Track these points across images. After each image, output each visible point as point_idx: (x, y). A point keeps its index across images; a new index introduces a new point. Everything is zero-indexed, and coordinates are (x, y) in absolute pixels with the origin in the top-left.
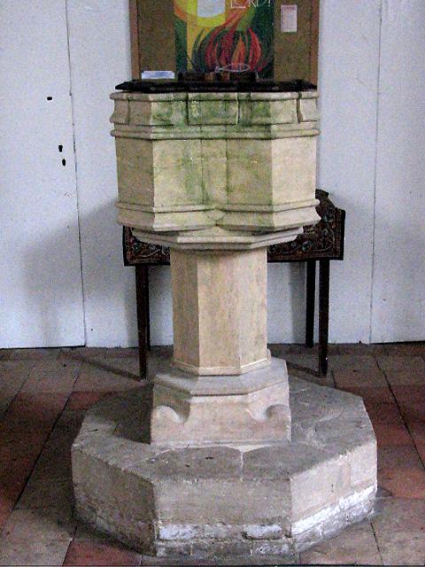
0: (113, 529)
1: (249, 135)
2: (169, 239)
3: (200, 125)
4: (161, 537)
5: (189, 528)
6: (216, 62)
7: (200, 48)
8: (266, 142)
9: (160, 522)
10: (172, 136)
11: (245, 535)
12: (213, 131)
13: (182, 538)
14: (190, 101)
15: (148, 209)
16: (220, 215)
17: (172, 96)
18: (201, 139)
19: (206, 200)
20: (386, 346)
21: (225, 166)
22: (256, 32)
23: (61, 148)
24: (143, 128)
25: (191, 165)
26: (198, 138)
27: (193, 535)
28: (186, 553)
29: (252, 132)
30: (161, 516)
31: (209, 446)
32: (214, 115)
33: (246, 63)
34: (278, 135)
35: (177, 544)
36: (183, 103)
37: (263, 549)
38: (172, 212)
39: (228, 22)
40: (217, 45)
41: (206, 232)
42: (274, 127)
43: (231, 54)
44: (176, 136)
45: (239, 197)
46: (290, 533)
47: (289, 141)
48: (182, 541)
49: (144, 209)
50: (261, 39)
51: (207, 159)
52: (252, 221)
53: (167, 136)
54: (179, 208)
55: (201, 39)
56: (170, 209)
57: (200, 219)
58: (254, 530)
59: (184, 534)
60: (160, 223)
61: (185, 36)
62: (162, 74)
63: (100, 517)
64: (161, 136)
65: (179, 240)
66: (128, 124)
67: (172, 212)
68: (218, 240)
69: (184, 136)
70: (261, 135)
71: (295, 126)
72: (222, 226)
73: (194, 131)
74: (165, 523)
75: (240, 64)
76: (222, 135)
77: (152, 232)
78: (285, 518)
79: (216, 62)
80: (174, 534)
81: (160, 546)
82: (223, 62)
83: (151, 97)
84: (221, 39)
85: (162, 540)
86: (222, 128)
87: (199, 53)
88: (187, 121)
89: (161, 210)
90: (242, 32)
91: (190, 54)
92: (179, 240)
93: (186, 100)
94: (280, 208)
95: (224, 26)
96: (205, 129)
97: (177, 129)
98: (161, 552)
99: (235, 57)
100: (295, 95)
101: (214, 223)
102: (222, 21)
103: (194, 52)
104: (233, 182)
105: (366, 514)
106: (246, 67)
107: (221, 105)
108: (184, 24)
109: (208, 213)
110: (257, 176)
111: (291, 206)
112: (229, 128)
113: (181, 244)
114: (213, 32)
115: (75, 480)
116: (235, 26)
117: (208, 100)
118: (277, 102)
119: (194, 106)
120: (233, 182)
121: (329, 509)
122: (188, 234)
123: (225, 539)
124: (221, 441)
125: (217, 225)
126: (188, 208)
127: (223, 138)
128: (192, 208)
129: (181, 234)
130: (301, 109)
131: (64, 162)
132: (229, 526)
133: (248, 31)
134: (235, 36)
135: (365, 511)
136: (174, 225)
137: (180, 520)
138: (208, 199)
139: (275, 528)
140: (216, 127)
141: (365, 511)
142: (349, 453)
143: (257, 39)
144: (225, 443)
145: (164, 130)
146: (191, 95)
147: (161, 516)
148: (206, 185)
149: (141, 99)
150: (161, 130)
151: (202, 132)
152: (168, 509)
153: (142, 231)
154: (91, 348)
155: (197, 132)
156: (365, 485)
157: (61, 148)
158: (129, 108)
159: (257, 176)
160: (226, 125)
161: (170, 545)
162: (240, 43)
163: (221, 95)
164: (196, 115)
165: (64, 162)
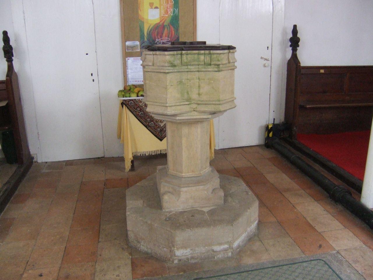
0: (149, 251)
1: (209, 70)
2: (174, 118)
3: (187, 65)
4: (176, 255)
5: (188, 250)
6: (156, 37)
7: (150, 31)
8: (217, 73)
9: (175, 249)
10: (176, 71)
11: (213, 251)
12: (192, 68)
13: (185, 254)
14: (183, 55)
15: (164, 105)
16: (195, 106)
17: (175, 52)
18: (188, 72)
19: (189, 100)
20: (225, 150)
21: (198, 83)
22: (172, 25)
23: (92, 74)
24: (162, 68)
25: (183, 84)
26: (186, 72)
27: (190, 253)
28: (187, 261)
29: (211, 68)
30: (176, 246)
31: (189, 210)
32: (194, 60)
33: (168, 37)
34: (223, 69)
35: (183, 258)
36: (180, 56)
37: (220, 256)
38: (175, 106)
39: (161, 21)
40: (157, 31)
41: (189, 114)
42: (221, 66)
43: (162, 34)
44: (177, 71)
45: (204, 98)
46: (232, 247)
47: (225, 72)
48: (185, 256)
49: (162, 105)
50: (174, 27)
51: (190, 80)
52: (211, 108)
53: (173, 71)
54: (178, 104)
55: (150, 29)
56: (173, 104)
57: (186, 108)
58: (217, 248)
59: (186, 253)
60: (170, 111)
61: (143, 28)
62: (134, 43)
63: (143, 245)
64: (171, 71)
65: (178, 118)
66: (153, 66)
67: (175, 106)
68: (195, 117)
69: (181, 70)
70: (216, 70)
71: (228, 65)
72: (196, 111)
73: (184, 68)
74: (178, 249)
75: (166, 38)
76: (197, 70)
77: (176, 120)
78: (231, 242)
79: (156, 37)
80: (181, 253)
81: (175, 259)
82: (159, 37)
83: (166, 53)
84: (159, 28)
85: (176, 256)
86: (197, 67)
87: (150, 33)
88: (182, 64)
89: (170, 105)
90: (166, 25)
91: (146, 34)
92: (178, 118)
93: (181, 54)
94: (224, 102)
95: (159, 23)
96: (189, 67)
97: (177, 68)
98: (176, 262)
99: (164, 35)
100: (179, 52)
101: (193, 110)
102: (158, 21)
103: (147, 33)
104: (201, 91)
105: (255, 232)
106: (168, 39)
107: (196, 56)
108: (143, 22)
109: (190, 106)
110: (213, 88)
111: (227, 101)
112: (200, 67)
113: (179, 120)
114: (155, 25)
115: (128, 229)
116: (164, 22)
117: (190, 54)
118: (222, 54)
119: (184, 57)
120: (201, 91)
121: (244, 234)
122: (182, 115)
123: (204, 253)
124: (194, 206)
125: (194, 111)
126: (182, 103)
127: (197, 71)
128: (184, 103)
129: (178, 115)
130: (230, 57)
131: (93, 80)
132: (206, 247)
133: (169, 25)
134: (163, 27)
135: (255, 231)
136: (176, 112)
137: (184, 247)
138: (190, 99)
139: (226, 246)
140: (194, 66)
141: (255, 231)
142: (250, 208)
143: (172, 27)
144: (196, 207)
145: (172, 68)
146: (184, 52)
147: (176, 246)
148: (189, 93)
149: (191, 53)
150: (169, 68)
151: (187, 68)
152: (179, 243)
153: (155, 114)
154: (107, 158)
155: (186, 69)
156: (254, 221)
157: (92, 74)
158: (154, 58)
159: (213, 88)
160: (198, 65)
161: (180, 258)
162: (166, 29)
163: (197, 52)
164: (186, 61)
165: (93, 80)
